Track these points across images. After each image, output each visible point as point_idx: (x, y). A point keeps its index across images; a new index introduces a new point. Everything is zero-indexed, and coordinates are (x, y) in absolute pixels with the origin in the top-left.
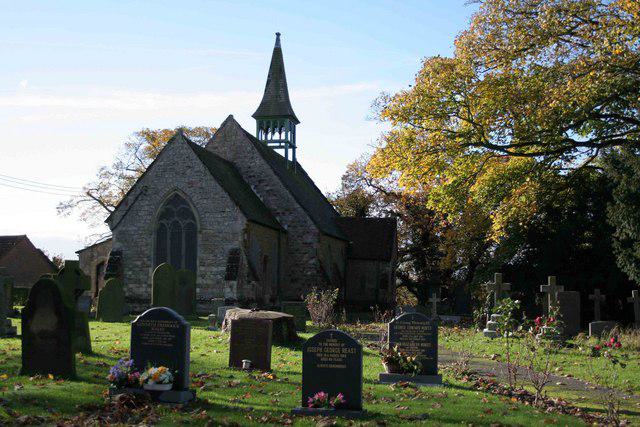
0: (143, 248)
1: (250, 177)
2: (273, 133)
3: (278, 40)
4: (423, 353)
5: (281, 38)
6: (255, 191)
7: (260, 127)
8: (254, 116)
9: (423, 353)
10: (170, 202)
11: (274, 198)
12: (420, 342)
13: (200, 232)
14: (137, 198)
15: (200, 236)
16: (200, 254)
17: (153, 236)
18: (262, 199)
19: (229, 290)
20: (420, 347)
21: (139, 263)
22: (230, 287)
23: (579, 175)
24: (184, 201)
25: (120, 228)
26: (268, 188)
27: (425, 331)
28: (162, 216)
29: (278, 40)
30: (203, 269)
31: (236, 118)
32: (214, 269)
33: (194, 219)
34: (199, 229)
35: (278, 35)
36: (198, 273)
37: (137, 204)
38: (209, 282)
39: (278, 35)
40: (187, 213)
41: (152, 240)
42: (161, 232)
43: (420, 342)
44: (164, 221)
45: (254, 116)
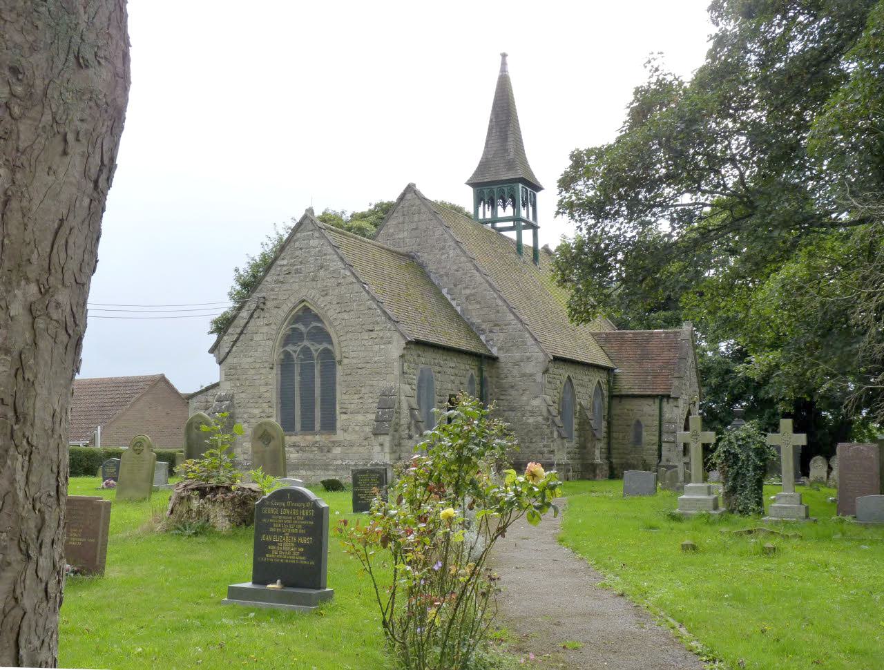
0: (262, 389)
1: (441, 276)
2: (504, 207)
3: (504, 64)
4: (301, 554)
5: (508, 59)
6: (449, 297)
7: (479, 200)
8: (471, 183)
9: (301, 554)
10: (297, 319)
11: (478, 306)
12: (297, 535)
13: (340, 362)
14: (251, 316)
15: (339, 368)
16: (340, 396)
17: (274, 371)
18: (458, 309)
19: (377, 449)
20: (298, 545)
21: (256, 411)
22: (382, 445)
23: (795, 184)
24: (317, 318)
25: (229, 360)
26: (468, 291)
27: (307, 518)
28: (288, 340)
29: (504, 64)
30: (344, 417)
31: (418, 187)
32: (360, 418)
33: (331, 342)
34: (338, 358)
35: (504, 56)
36: (338, 424)
37: (251, 323)
38: (354, 437)
39: (504, 56)
40: (321, 335)
41: (273, 377)
42: (286, 364)
43: (297, 535)
44: (290, 348)
45: (471, 183)
